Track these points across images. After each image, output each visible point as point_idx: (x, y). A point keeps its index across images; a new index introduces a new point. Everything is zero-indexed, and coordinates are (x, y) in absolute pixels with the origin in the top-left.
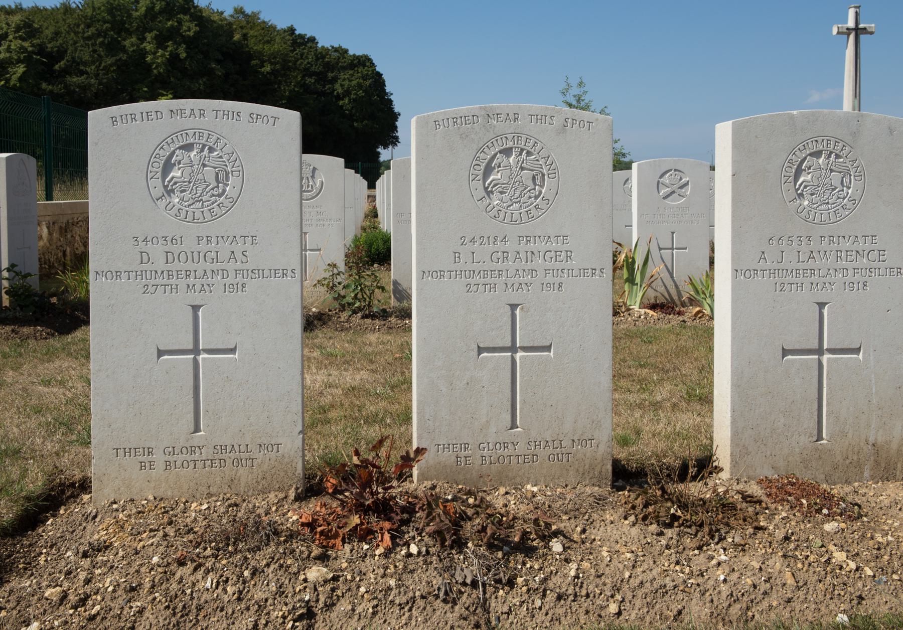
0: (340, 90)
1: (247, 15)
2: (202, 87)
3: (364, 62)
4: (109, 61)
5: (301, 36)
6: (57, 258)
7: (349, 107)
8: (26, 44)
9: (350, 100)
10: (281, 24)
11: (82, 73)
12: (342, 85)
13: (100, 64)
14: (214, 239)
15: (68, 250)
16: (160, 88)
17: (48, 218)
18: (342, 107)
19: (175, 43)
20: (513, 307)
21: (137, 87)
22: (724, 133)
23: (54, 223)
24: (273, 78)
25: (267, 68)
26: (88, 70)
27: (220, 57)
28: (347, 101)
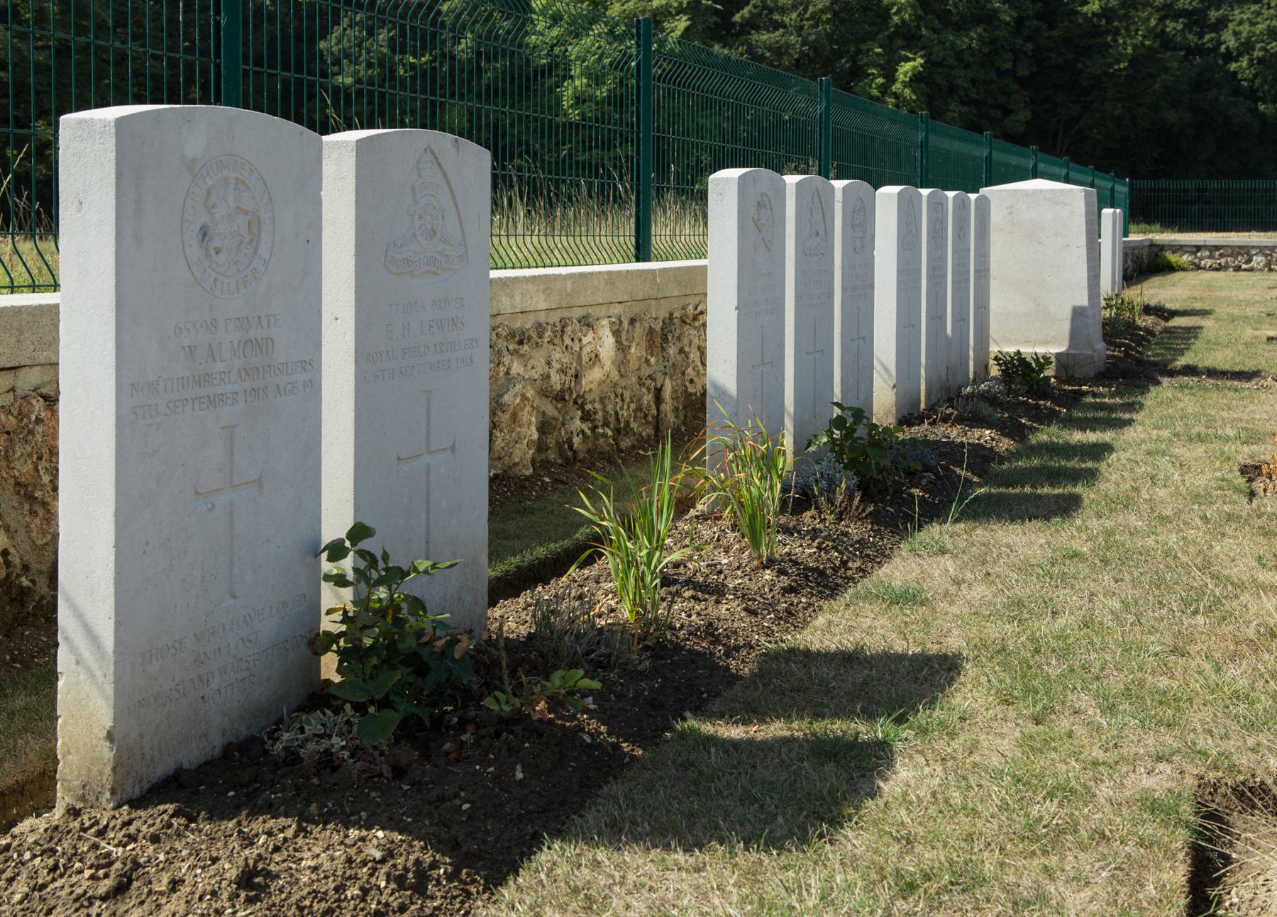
0: (1232, 43)
2: (974, 44)
6: (639, 409)
7: (1249, 73)
9: (1251, 60)
11: (777, 26)
12: (1236, 34)
13: (805, 10)
15: (668, 387)
16: (903, 48)
17: (616, 310)
18: (1235, 73)
21: (863, 47)
22: (494, 274)
23: (632, 321)
24: (1103, 22)
26: (786, 20)
28: (1245, 62)
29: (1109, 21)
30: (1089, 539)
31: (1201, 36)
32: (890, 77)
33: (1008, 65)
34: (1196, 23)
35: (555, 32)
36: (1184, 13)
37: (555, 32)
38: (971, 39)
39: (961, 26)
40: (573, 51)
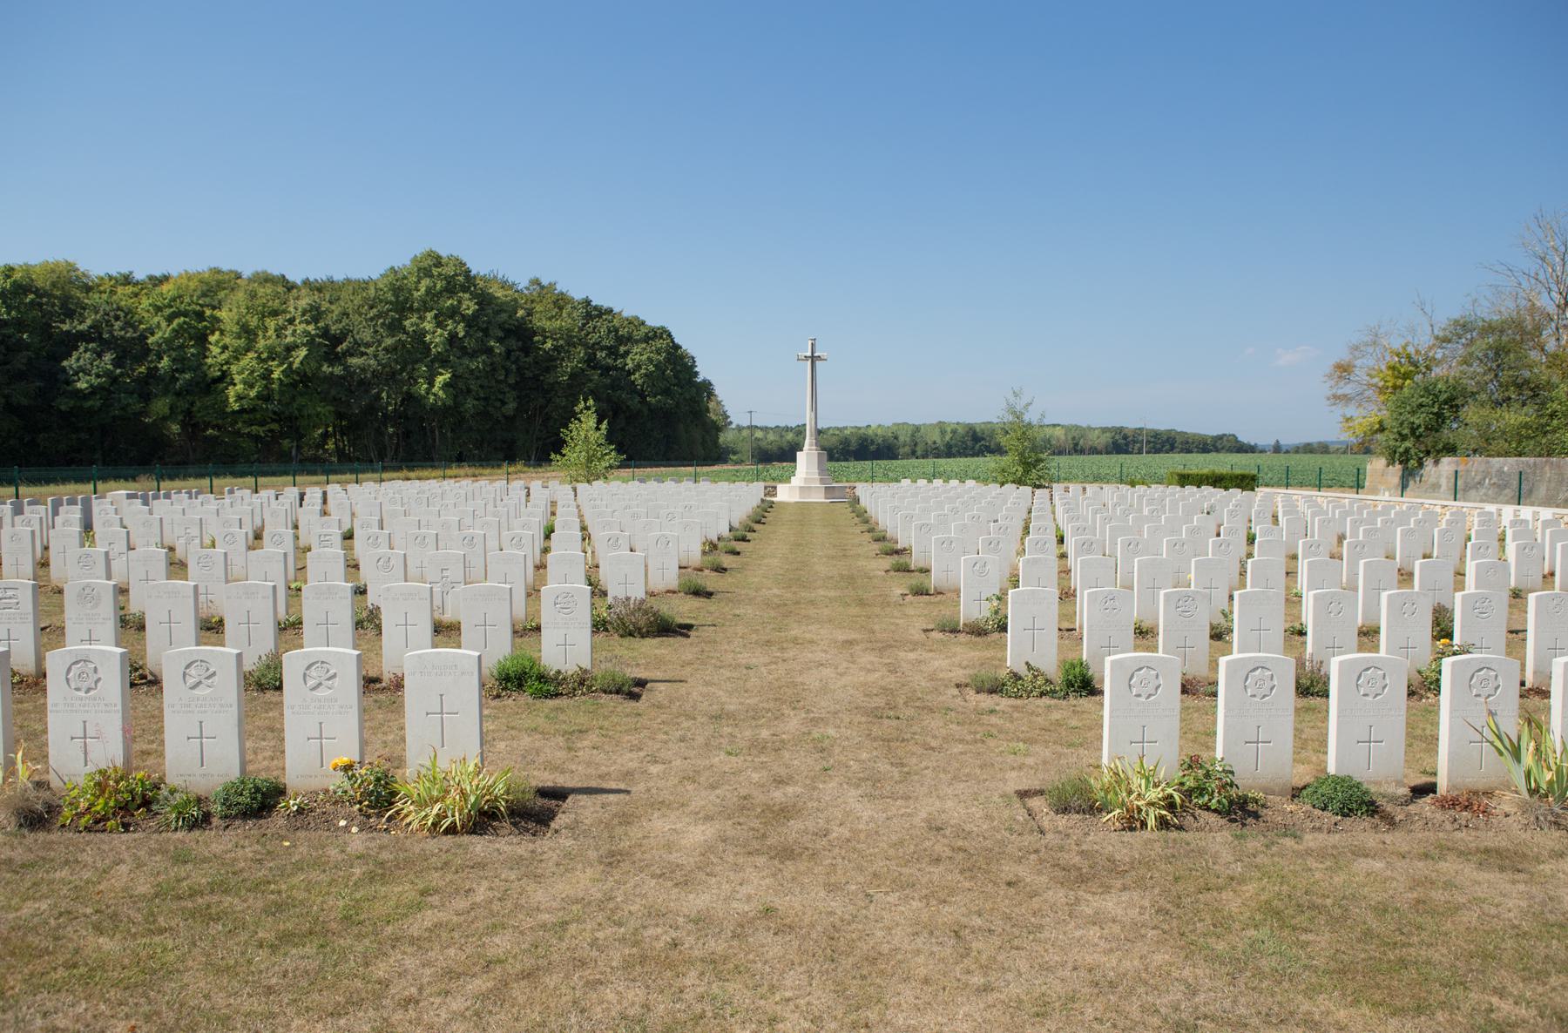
1: (543, 288)
3: (661, 334)
4: (389, 341)
5: (596, 308)
8: (311, 328)
10: (577, 295)
11: (363, 354)
25: (549, 345)
27: (500, 334)
30: (814, 788)
32: (431, 384)
35: (224, 356)
36: (607, 348)
37: (224, 356)
38: (477, 364)
39: (473, 355)
40: (234, 369)
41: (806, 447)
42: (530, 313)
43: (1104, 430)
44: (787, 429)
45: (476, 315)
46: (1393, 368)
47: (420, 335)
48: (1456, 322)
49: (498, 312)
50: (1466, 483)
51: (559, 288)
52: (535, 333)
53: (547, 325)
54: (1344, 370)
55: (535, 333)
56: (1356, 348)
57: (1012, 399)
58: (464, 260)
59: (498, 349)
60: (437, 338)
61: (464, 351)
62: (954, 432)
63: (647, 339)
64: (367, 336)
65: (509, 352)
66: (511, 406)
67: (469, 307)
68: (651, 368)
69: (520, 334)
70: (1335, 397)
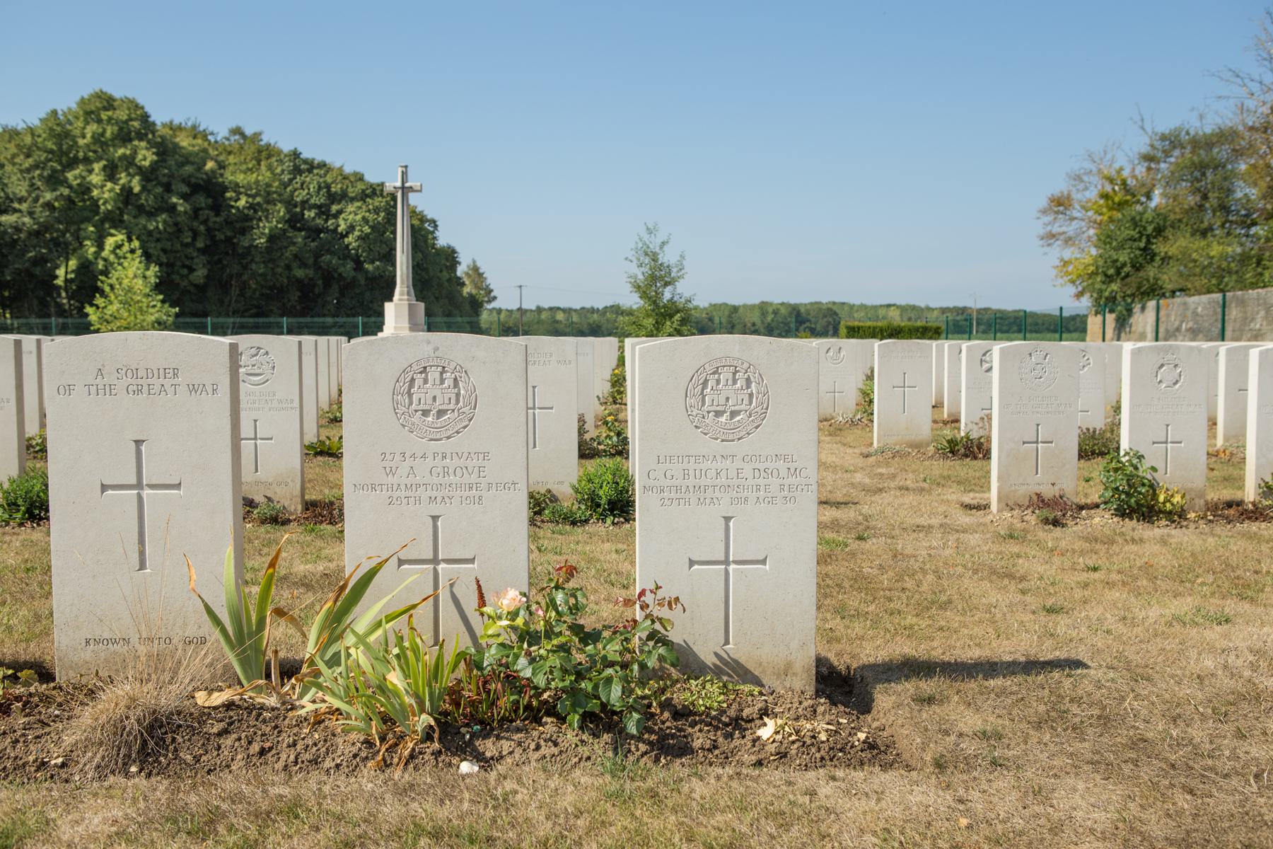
2: (160, 226)
5: (305, 161)
11: (16, 211)
14: (449, 456)
18: (347, 246)
19: (129, 174)
20: (727, 519)
25: (242, 202)
27: (185, 189)
29: (256, 211)
31: (326, 221)
32: (101, 247)
33: (189, 240)
34: (323, 213)
36: (319, 207)
39: (151, 215)
41: (396, 297)
42: (222, 166)
43: (944, 310)
44: (593, 311)
45: (154, 167)
46: (1105, 196)
47: (85, 189)
48: (1163, 138)
49: (182, 165)
50: (1167, 331)
51: (265, 139)
52: (226, 189)
53: (240, 178)
54: (1060, 204)
55: (226, 189)
56: (1079, 178)
57: (646, 237)
58: (141, 101)
59: (181, 206)
60: (105, 193)
61: (141, 210)
62: (776, 312)
63: (363, 196)
64: (21, 189)
65: (196, 211)
66: (200, 274)
67: (146, 157)
68: (367, 229)
69: (210, 190)
70: (1052, 236)
